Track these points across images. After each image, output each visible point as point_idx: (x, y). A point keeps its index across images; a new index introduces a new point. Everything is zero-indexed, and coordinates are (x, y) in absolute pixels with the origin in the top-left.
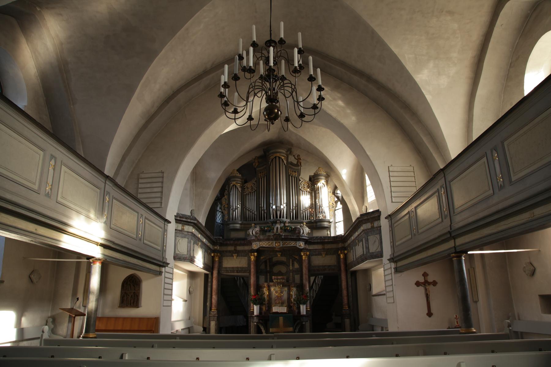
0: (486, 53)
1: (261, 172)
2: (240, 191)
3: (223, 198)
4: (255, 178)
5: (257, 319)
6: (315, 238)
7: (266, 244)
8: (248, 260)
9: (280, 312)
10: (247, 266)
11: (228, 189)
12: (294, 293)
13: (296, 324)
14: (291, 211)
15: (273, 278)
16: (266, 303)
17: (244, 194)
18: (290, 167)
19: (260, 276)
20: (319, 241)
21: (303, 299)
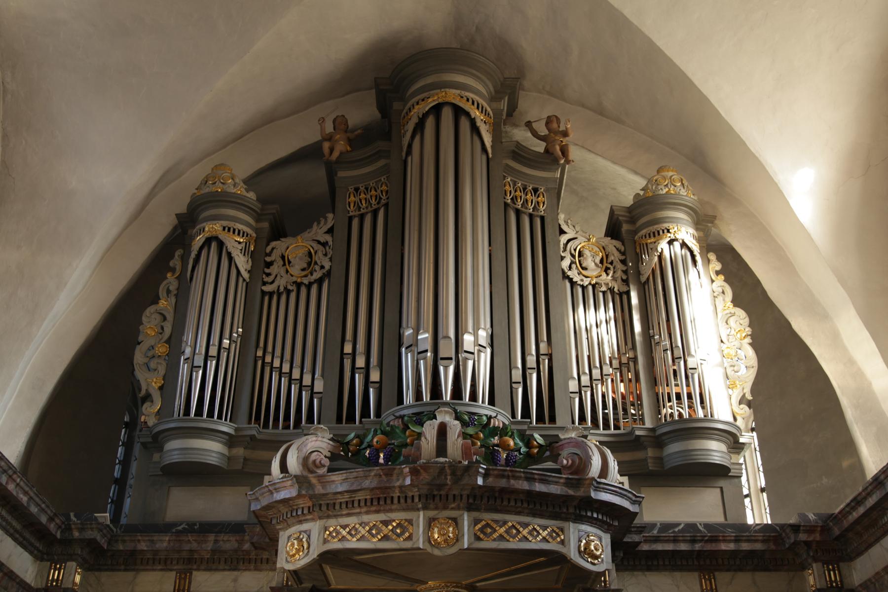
1: (362, 189)
2: (246, 275)
3: (152, 309)
4: (330, 216)
6: (655, 532)
7: (363, 531)
11: (178, 268)
14: (517, 375)
17: (267, 288)
18: (510, 170)
20: (683, 547)
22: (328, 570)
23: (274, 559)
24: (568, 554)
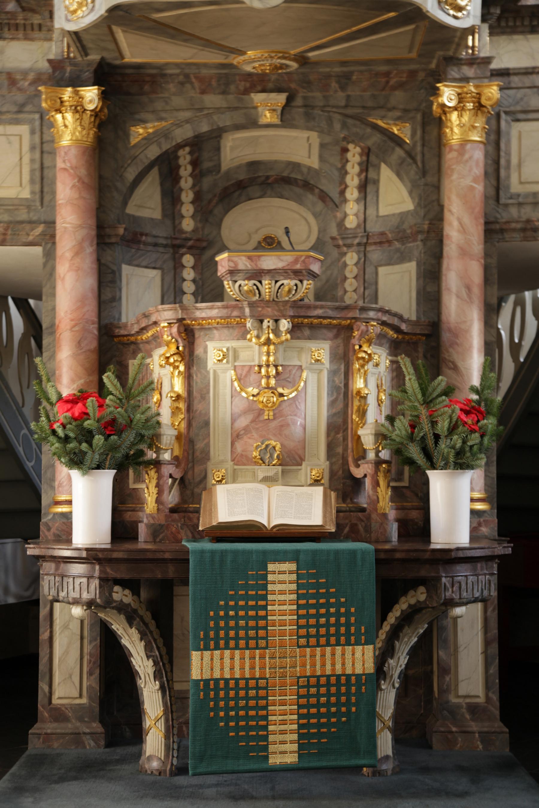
0: (217, 505)
5: (89, 578)
8: (33, 148)
9: (273, 524)
10: (26, 194)
12: (379, 387)
13: (392, 618)
15: (222, 270)
16: (166, 456)
19: (126, 269)
21: (452, 429)
22: (120, 34)
23: (49, 24)
24: (424, 5)
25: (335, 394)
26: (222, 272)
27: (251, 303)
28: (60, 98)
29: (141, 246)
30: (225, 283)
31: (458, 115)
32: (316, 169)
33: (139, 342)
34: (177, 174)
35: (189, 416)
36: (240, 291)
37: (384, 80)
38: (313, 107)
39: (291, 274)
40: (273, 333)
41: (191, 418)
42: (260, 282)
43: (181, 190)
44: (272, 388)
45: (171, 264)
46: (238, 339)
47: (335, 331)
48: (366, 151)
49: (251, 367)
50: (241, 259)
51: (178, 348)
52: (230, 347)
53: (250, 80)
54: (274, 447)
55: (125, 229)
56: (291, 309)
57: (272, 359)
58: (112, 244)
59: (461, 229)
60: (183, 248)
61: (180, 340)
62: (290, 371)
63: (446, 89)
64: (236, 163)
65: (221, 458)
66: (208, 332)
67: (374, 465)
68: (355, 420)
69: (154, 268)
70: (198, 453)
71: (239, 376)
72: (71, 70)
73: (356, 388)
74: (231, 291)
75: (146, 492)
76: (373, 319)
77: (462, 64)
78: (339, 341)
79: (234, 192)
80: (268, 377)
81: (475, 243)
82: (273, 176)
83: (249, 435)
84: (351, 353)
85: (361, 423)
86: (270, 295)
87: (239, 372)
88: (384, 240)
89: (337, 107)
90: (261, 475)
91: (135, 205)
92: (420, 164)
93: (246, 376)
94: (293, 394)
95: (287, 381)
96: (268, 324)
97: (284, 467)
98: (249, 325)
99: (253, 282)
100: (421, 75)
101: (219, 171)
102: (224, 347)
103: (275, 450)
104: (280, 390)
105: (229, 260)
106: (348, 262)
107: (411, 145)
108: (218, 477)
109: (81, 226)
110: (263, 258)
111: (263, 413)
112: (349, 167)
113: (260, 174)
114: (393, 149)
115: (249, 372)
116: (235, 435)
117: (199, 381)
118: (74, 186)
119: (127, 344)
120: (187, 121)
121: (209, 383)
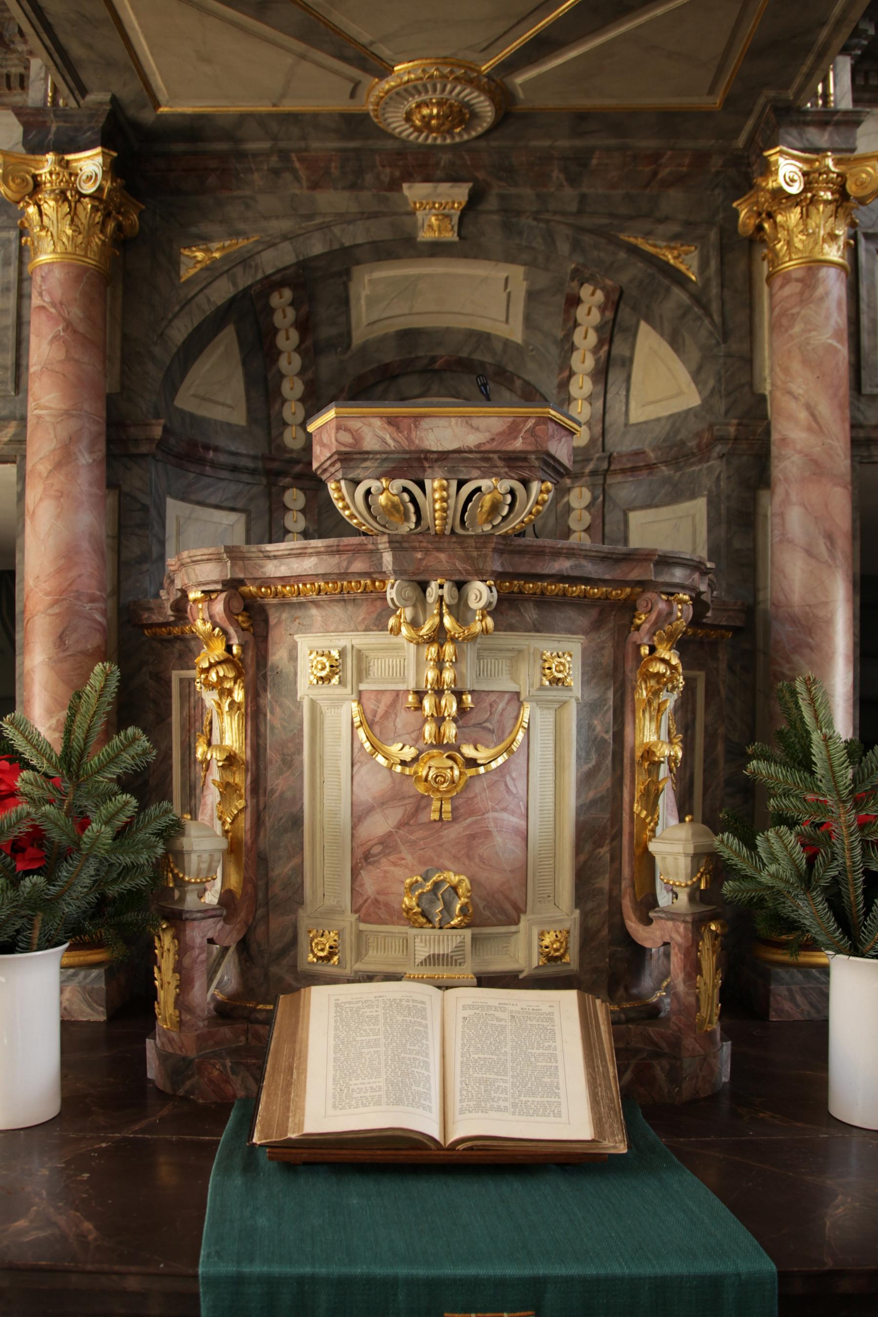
9: (453, 1137)
19: (174, 508)
25: (594, 757)
26: (323, 459)
27: (398, 538)
28: (35, 177)
29: (207, 468)
30: (331, 486)
31: (802, 213)
32: (518, 344)
33: (187, 636)
34: (273, 345)
35: (258, 802)
36: (368, 507)
37: (648, 169)
38: (519, 213)
39: (500, 463)
40: (450, 613)
41: (261, 807)
42: (421, 486)
43: (281, 376)
44: (449, 747)
45: (262, 504)
46: (367, 629)
47: (594, 613)
48: (616, 297)
49: (397, 695)
50: (370, 425)
51: (229, 649)
52: (349, 647)
53: (401, 163)
54: (454, 888)
55: (165, 429)
56: (496, 556)
57: (448, 676)
58: (143, 456)
59: (814, 425)
60: (286, 477)
61: (231, 630)
62: (491, 705)
63: (782, 161)
64: (379, 331)
65: (330, 902)
66: (299, 613)
67: (690, 926)
68: (638, 815)
69: (233, 509)
70: (276, 889)
71: (370, 716)
72: (58, 128)
73: (642, 743)
74: (346, 507)
75: (156, 975)
76: (683, 587)
77: (807, 124)
78: (604, 636)
79: (376, 384)
80: (439, 720)
81: (840, 451)
82: (442, 357)
83: (392, 858)
84: (630, 664)
85: (651, 821)
86: (444, 519)
87: (370, 705)
88: (641, 464)
89: (563, 213)
90: (422, 952)
91: (194, 396)
92: (717, 318)
93: (386, 715)
94: (500, 760)
95: (485, 728)
96: (440, 592)
97: (477, 930)
98: (391, 594)
99: (399, 483)
100: (716, 163)
101: (349, 345)
102: (334, 647)
103: (457, 893)
104: (469, 751)
105: (338, 428)
106: (574, 503)
107: (700, 284)
108: (322, 950)
109: (67, 414)
110: (425, 423)
111: (429, 805)
112: (578, 337)
113: (421, 353)
114: (668, 290)
115: (394, 704)
116: (359, 853)
117: (277, 724)
118: (56, 338)
119: (169, 641)
120: (285, 238)
121: (301, 730)
